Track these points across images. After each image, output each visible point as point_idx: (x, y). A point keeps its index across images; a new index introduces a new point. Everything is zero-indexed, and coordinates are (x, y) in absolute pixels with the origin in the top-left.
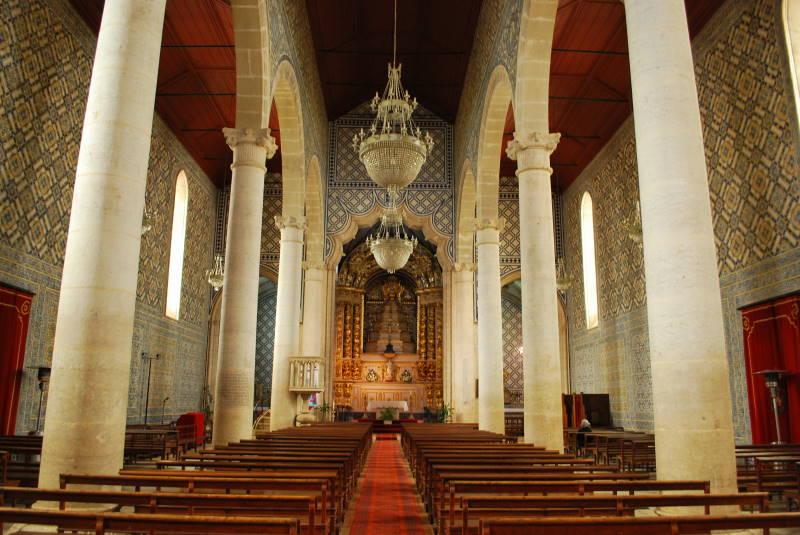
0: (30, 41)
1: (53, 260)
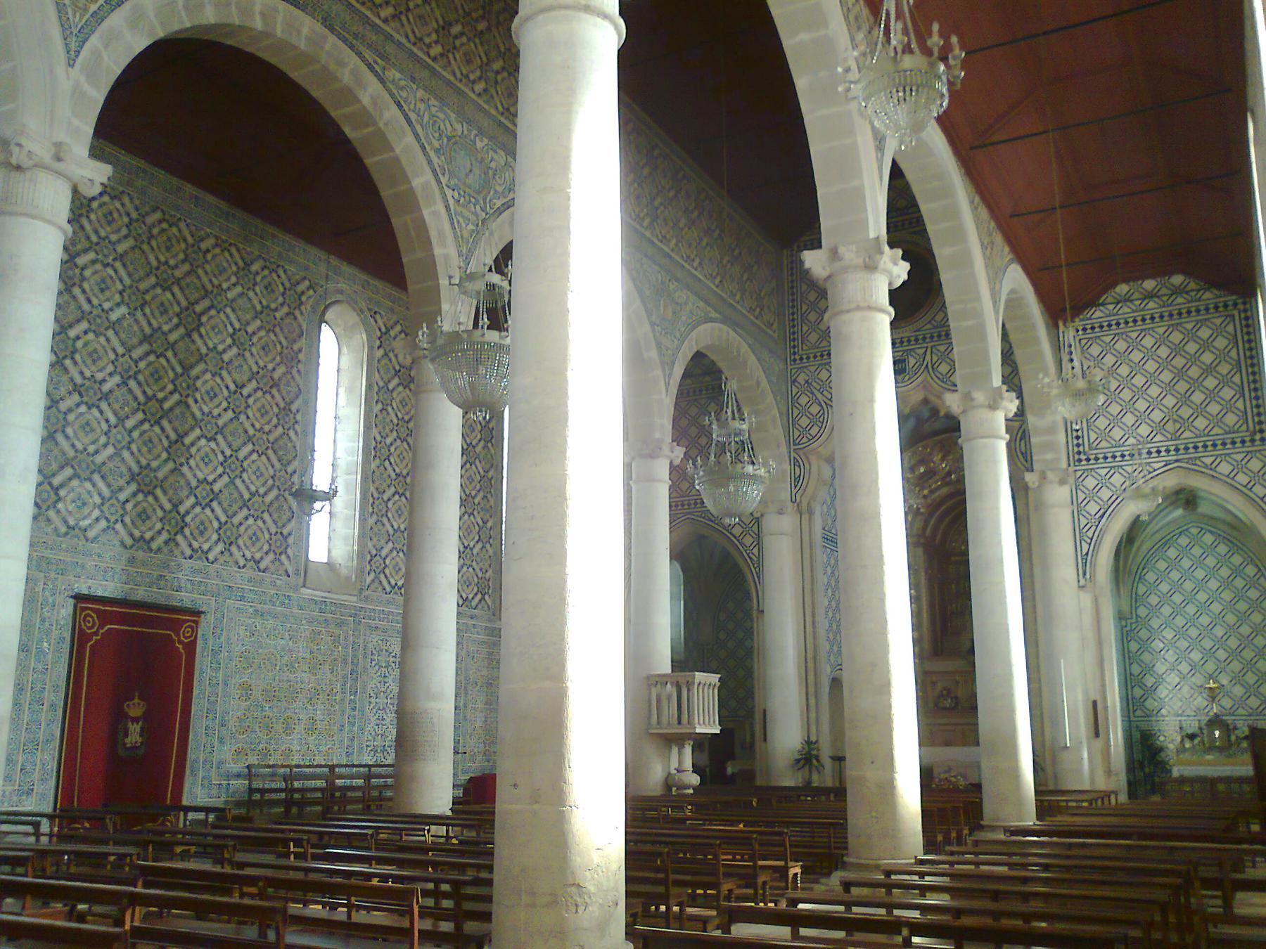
1: (237, 563)
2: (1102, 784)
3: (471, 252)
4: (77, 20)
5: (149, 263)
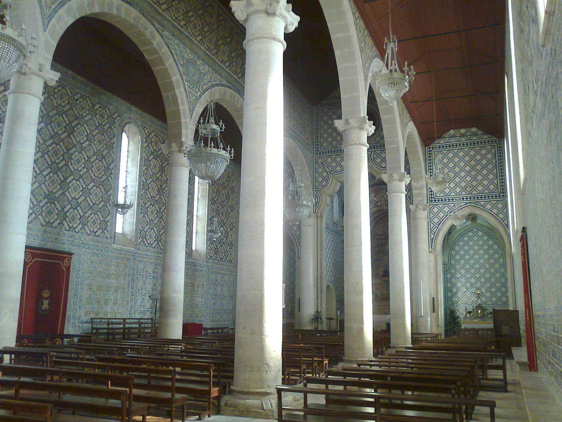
0: (57, 110)
1: (87, 233)
2: (435, 331)
3: (194, 108)
4: (47, 12)
5: (54, 105)
